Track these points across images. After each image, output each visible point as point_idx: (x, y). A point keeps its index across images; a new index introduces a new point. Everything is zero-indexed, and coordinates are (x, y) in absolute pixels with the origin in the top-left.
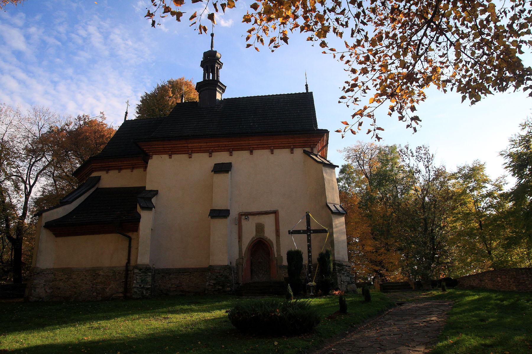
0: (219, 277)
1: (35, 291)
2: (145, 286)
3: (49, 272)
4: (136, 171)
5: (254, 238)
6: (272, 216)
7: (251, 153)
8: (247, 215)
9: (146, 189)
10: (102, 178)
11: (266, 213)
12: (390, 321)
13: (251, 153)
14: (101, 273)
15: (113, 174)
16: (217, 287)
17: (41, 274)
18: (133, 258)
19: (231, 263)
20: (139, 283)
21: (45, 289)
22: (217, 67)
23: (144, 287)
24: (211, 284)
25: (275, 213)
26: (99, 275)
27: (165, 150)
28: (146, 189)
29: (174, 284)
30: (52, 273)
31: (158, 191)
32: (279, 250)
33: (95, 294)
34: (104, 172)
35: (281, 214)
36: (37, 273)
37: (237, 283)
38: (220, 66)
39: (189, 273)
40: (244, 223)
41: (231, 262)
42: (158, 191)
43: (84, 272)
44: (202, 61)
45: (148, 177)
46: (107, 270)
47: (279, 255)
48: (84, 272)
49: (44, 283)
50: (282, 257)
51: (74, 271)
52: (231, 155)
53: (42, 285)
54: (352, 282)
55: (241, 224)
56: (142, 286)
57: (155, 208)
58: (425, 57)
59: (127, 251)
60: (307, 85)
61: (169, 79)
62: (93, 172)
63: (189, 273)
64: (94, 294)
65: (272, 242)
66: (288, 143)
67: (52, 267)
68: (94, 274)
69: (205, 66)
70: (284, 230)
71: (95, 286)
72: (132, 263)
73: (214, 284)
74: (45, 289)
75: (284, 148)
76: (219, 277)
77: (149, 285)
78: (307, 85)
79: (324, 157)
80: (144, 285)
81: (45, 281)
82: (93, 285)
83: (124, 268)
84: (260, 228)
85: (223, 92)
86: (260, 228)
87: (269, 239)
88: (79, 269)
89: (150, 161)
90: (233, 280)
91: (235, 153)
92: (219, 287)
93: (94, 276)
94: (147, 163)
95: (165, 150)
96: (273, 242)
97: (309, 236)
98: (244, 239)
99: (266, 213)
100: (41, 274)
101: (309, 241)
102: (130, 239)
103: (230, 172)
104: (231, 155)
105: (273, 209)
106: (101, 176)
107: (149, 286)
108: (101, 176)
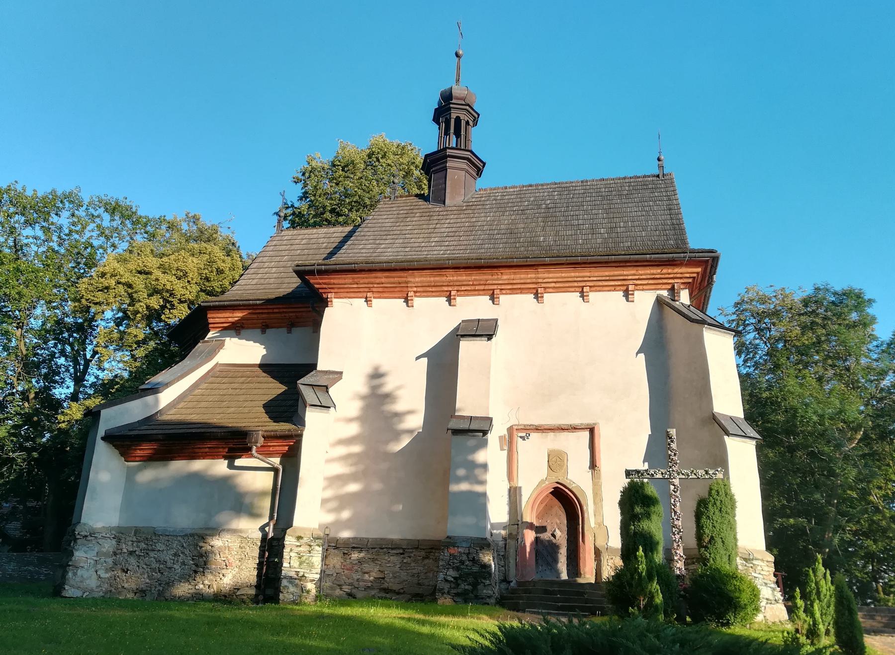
0: (467, 563)
1: (75, 574)
3: (108, 535)
4: (297, 332)
5: (542, 482)
11: (574, 428)
17: (89, 538)
20: (295, 568)
22: (458, 120)
24: (449, 578)
27: (359, 288)
29: (367, 573)
36: (81, 535)
37: (505, 580)
38: (474, 120)
39: (401, 551)
40: (521, 446)
44: (436, 110)
47: (600, 524)
49: (95, 558)
53: (92, 561)
54: (776, 600)
57: (335, 408)
61: (879, 319)
66: (555, 282)
73: (455, 578)
74: (96, 572)
76: (467, 563)
79: (433, 588)
84: (556, 460)
85: (477, 175)
86: (556, 460)
91: (503, 299)
95: (359, 288)
99: (574, 428)
100: (89, 538)
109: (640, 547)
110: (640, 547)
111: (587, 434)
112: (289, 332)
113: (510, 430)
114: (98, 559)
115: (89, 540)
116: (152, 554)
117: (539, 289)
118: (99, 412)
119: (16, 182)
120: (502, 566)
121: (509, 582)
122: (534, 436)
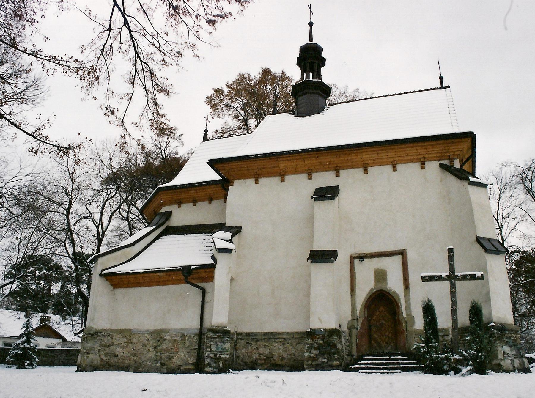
2: (222, 356)
4: (216, 203)
5: (372, 289)
6: (399, 258)
7: (366, 171)
8: (361, 257)
9: (226, 226)
10: (173, 214)
11: (390, 254)
12: (9, 218)
13: (366, 171)
14: (167, 337)
15: (187, 207)
16: (320, 359)
18: (206, 316)
19: (340, 326)
20: (214, 351)
21: (100, 356)
23: (220, 357)
25: (402, 253)
26: (165, 340)
28: (226, 226)
30: (109, 336)
31: (241, 227)
32: (408, 307)
33: (158, 364)
34: (176, 206)
35: (411, 255)
39: (283, 340)
41: (340, 325)
42: (241, 227)
43: (146, 335)
45: (228, 207)
46: (175, 333)
47: (409, 315)
48: (146, 335)
50: (413, 316)
51: (134, 334)
52: (338, 175)
55: (387, 252)
56: (218, 356)
58: (217, 350)
59: (200, 308)
60: (441, 78)
62: (163, 205)
63: (283, 340)
64: (157, 365)
65: (397, 295)
67: (109, 328)
68: (158, 339)
69: (303, 64)
70: (414, 278)
71: (160, 354)
72: (207, 324)
74: (100, 356)
75: (411, 161)
77: (228, 355)
78: (441, 78)
80: (220, 354)
81: (100, 345)
82: (157, 352)
83: (199, 331)
87: (394, 292)
88: (140, 331)
89: (231, 188)
90: (344, 350)
92: (323, 360)
93: (158, 341)
94: (227, 191)
96: (400, 295)
97: (453, 286)
98: (358, 291)
99: (390, 254)
100: (95, 336)
101: (453, 294)
102: (204, 292)
103: (336, 199)
104: (338, 175)
105: (399, 247)
106: (172, 211)
107: (228, 357)
108: (172, 211)
109: (229, 369)
110: (229, 369)
111: (399, 258)
112: (194, 205)
113: (353, 258)
114: (100, 348)
115: (95, 337)
116: (130, 345)
117: (450, 156)
118: (218, 248)
119: (117, 125)
120: (348, 346)
121: (353, 355)
122: (366, 260)
